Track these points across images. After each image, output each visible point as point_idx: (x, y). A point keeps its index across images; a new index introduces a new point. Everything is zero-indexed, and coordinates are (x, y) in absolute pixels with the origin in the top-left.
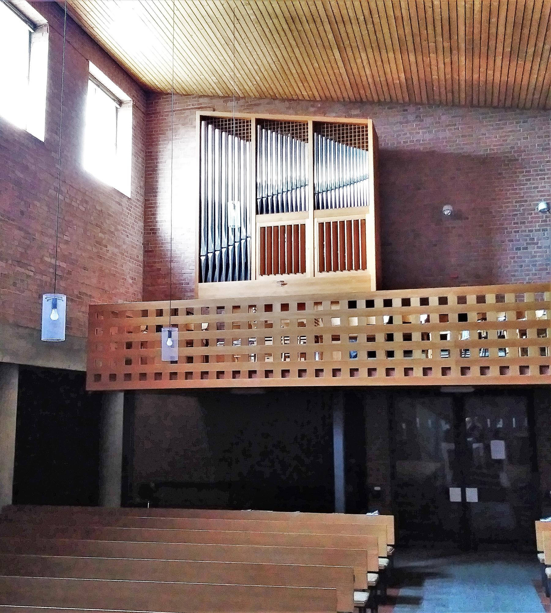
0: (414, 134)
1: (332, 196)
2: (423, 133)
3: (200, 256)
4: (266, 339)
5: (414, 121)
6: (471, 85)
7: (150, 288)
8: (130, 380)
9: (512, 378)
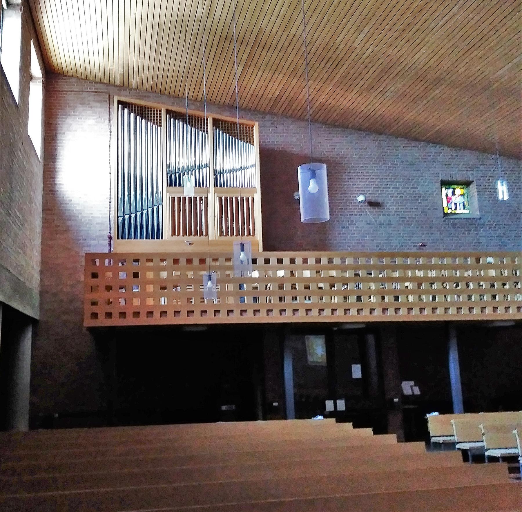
0: (291, 138)
1: (227, 178)
2: (277, 136)
3: (118, 217)
4: (188, 287)
5: (269, 127)
6: (322, 105)
7: (49, 242)
8: (111, 318)
9: (326, 317)
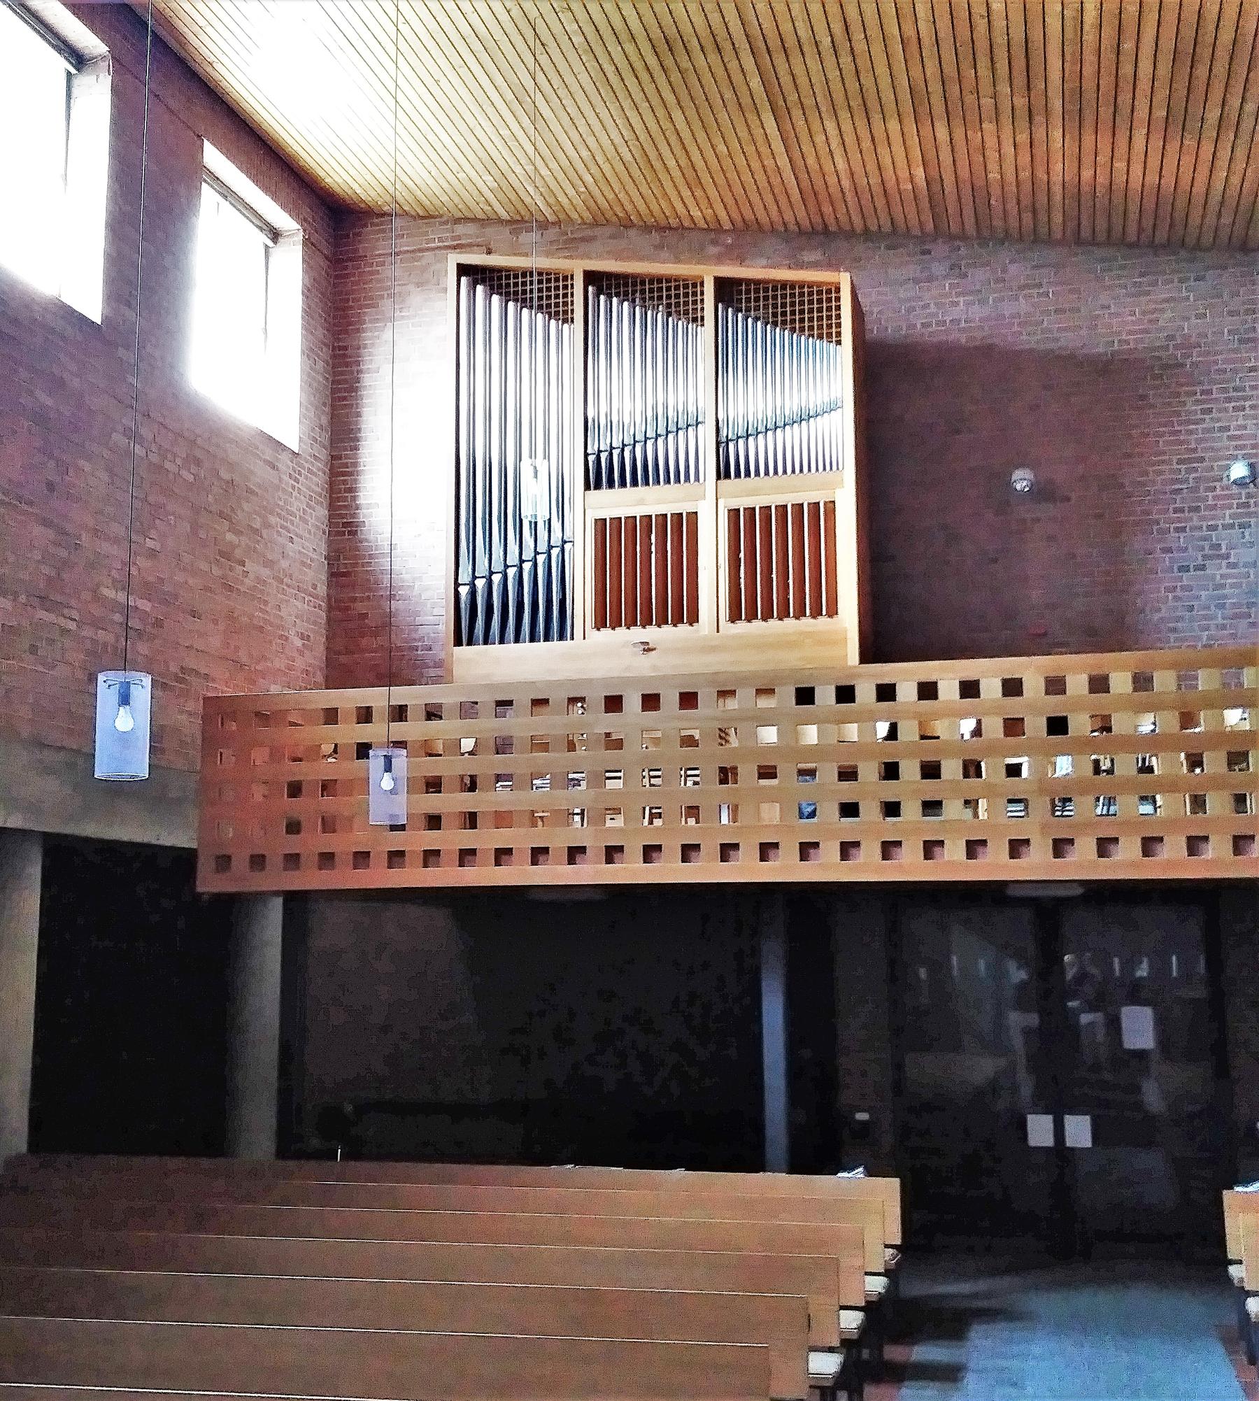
0: (945, 305)
1: (758, 448)
2: (967, 304)
3: (457, 585)
4: (608, 775)
5: (946, 277)
6: (1075, 194)
7: (343, 659)
8: (297, 868)
9: (1170, 864)
